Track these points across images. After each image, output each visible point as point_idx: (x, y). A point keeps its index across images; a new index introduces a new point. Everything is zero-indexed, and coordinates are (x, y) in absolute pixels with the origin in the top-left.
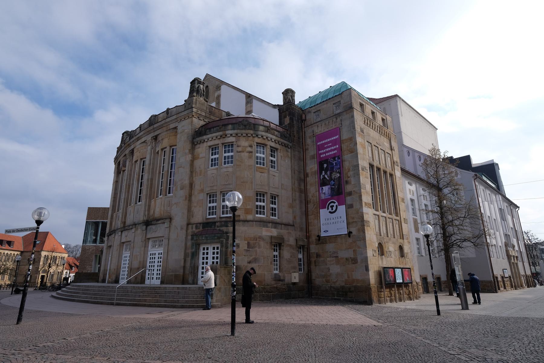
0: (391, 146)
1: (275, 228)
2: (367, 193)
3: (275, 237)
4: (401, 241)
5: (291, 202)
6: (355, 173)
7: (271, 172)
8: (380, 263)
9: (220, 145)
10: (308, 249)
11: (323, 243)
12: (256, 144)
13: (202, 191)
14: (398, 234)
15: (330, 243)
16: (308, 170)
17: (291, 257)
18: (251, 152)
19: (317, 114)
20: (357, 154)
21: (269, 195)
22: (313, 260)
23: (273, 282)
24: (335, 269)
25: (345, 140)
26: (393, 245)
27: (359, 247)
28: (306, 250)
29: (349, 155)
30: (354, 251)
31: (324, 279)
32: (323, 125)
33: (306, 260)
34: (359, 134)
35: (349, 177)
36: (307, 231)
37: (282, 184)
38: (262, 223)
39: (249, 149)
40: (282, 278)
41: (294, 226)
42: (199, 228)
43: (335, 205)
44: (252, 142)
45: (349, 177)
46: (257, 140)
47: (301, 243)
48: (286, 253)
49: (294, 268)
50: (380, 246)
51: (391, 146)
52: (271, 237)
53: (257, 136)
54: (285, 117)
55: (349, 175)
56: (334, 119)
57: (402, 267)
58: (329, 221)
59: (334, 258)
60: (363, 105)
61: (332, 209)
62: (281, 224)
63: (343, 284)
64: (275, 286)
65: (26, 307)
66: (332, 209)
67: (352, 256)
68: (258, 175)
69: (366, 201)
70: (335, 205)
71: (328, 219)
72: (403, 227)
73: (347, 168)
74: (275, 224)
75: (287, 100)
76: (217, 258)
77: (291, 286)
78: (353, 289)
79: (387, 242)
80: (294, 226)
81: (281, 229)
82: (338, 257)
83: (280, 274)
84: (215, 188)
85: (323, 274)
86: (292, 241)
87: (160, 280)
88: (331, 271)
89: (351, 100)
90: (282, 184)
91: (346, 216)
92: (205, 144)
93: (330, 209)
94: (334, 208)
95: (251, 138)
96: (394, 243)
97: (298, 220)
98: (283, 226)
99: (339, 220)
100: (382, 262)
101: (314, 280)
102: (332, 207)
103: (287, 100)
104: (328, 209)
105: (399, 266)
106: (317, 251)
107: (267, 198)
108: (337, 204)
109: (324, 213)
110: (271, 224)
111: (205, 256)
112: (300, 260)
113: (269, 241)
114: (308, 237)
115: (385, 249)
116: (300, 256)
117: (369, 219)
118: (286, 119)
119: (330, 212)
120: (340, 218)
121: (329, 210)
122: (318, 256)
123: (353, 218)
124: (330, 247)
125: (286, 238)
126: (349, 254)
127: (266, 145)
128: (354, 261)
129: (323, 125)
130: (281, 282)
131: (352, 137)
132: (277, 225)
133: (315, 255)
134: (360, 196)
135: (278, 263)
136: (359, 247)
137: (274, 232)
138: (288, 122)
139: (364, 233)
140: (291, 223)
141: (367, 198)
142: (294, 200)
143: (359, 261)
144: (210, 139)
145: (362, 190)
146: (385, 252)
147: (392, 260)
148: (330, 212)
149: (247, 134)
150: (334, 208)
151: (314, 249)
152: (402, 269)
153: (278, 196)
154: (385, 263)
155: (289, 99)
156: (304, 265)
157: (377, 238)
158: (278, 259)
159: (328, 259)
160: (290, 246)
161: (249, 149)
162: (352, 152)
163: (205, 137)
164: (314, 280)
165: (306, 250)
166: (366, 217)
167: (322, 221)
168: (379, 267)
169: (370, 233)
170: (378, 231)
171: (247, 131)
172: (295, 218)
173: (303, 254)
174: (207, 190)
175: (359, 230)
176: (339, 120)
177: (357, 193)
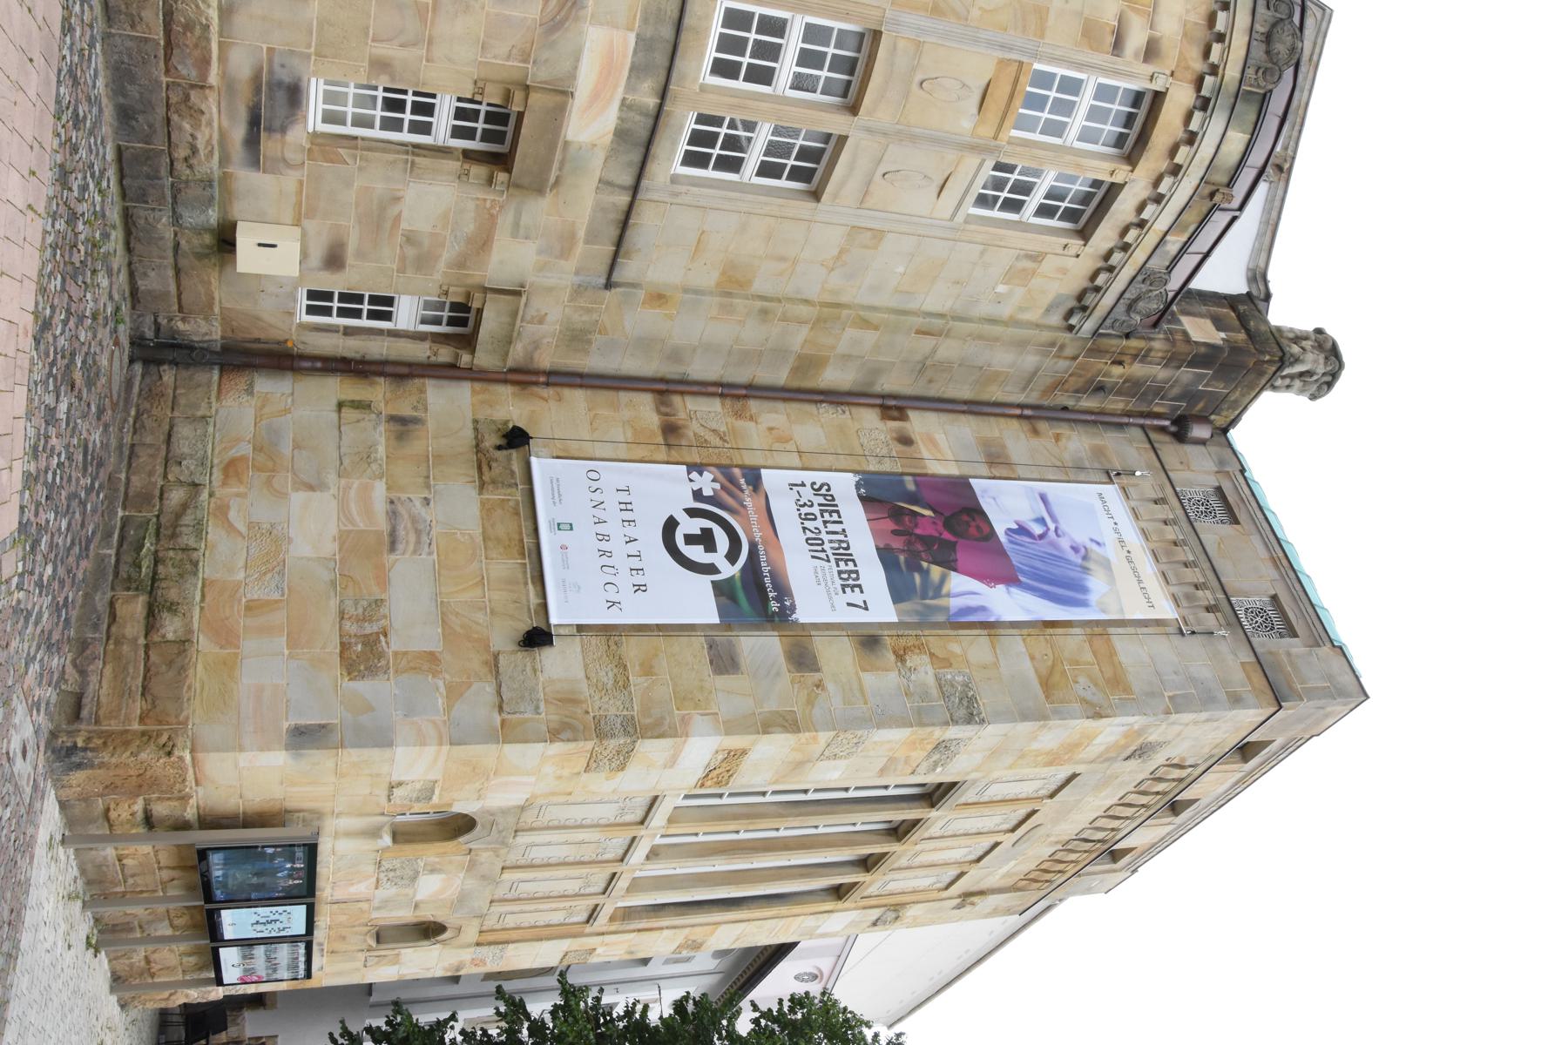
0: (981, 893)
1: (621, 134)
2: (799, 765)
3: (558, 114)
4: (471, 934)
5: (759, 286)
6: (925, 696)
7: (972, 161)
8: (345, 823)
10: (450, 372)
11: (482, 462)
12: (1157, 86)
14: (510, 921)
15: (487, 510)
16: (920, 423)
17: (410, 239)
18: (1118, 46)
19: (1215, 503)
20: (1042, 717)
21: (837, 123)
22: (377, 391)
23: (242, 64)
24: (312, 525)
25: (1112, 653)
26: (452, 892)
27: (454, 693)
28: (445, 354)
29: (1027, 667)
30: (432, 657)
31: (245, 449)
32: (1171, 533)
33: (377, 349)
34: (1139, 733)
35: (900, 658)
36: (561, 378)
37: (879, 235)
38: (667, 32)
39: (1136, 39)
40: (268, 145)
41: (609, 285)
43: (718, 558)
44: (1171, 64)
45: (900, 658)
46: (1180, 97)
47: (491, 322)
48: (438, 201)
49: (334, 260)
50: (458, 826)
51: (981, 893)
52: (562, 93)
53: (1204, 104)
54: (1219, 324)
55: (913, 660)
56: (1206, 597)
57: (319, 935)
58: (612, 513)
59: (383, 524)
60: (1245, 759)
61: (690, 540)
62: (635, 189)
63: (207, 570)
64: (213, 78)
66: (690, 540)
67: (394, 644)
68: (978, 66)
69: (752, 756)
70: (718, 558)
71: (626, 507)
72: (546, 945)
73: (955, 648)
74: (641, 141)
75: (1295, 349)
77: (213, 216)
78: (171, 627)
79: (472, 865)
80: (609, 285)
81: (604, 183)
82: (393, 546)
83: (296, 136)
85: (286, 449)
86: (511, 258)
88: (298, 498)
89: (1311, 693)
90: (879, 235)
91: (659, 627)
93: (694, 526)
94: (696, 553)
95: (1198, 66)
96: (462, 899)
97: (639, 319)
98: (624, 199)
99: (625, 581)
100: (349, 834)
101: (250, 391)
102: (706, 540)
103: (1295, 349)
104: (692, 513)
105: (322, 922)
106: (431, 425)
108: (728, 571)
109: (668, 489)
110: (652, 102)
112: (383, 306)
113: (538, 74)
114: (524, 377)
115: (431, 852)
116: (406, 314)
117: (633, 769)
118: (1208, 324)
119: (670, 525)
120: (639, 588)
121: (682, 518)
122: (403, 426)
123: (648, 670)
124: (459, 506)
125: (539, 211)
126: (411, 617)
127: (1132, 159)
128: (363, 654)
129: (1171, 533)
130: (239, 133)
131: (1127, 689)
132: (636, 157)
133: (406, 411)
134: (790, 724)
135: (377, 133)
136: (454, 693)
137: (591, 125)
138: (1196, 336)
139: (554, 735)
140: (629, 270)
141: (768, 762)
142: (767, 308)
143: (364, 687)
145: (824, 737)
146: (409, 849)
147: (362, 888)
148: (670, 525)
149: (1220, 38)
151: (450, 407)
152: (307, 939)
153: (816, 195)
154: (345, 846)
155: (1297, 360)
156: (348, 331)
157: (505, 812)
158: (405, 136)
159: (380, 490)
160: (482, 243)
161: (1136, 39)
162: (1047, 684)
164: (250, 391)
165: (445, 354)
166: (651, 750)
167: (614, 474)
168: (319, 815)
169: (549, 769)
170: (544, 820)
171: (1239, 42)
172: (659, 298)
173: (421, 337)
176: (1210, 620)
177: (810, 702)
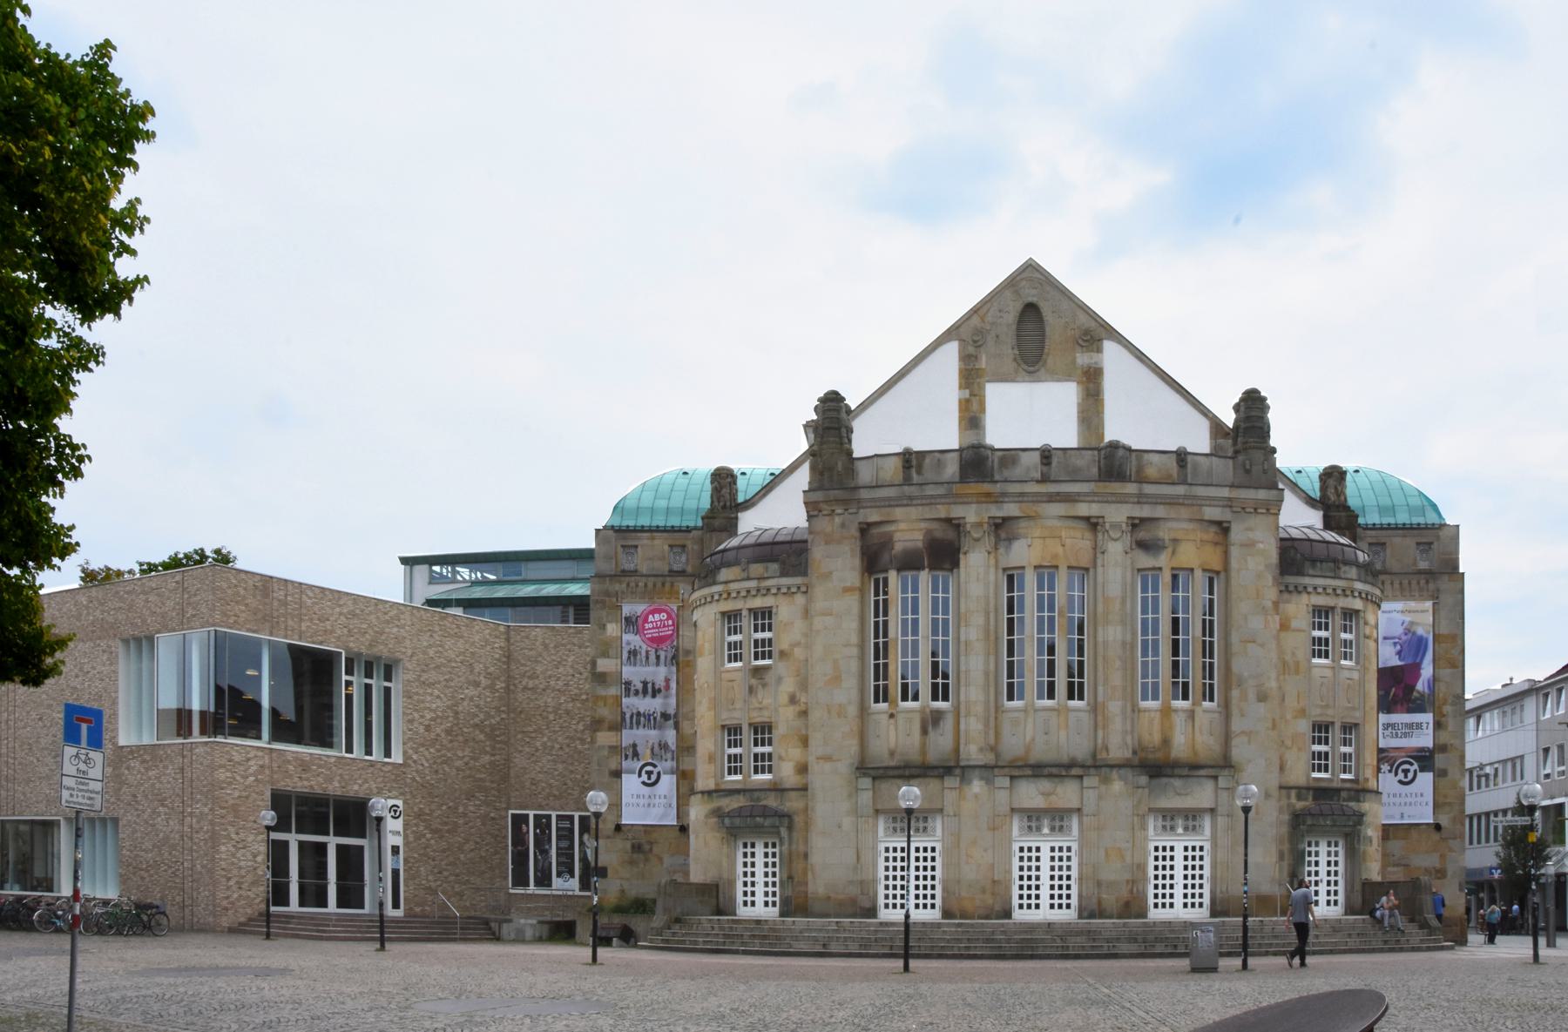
9: (745, 613)
13: (1302, 713)
27: (1451, 850)
42: (1306, 799)
43: (1412, 769)
65: (79, 986)
70: (1412, 769)
76: (774, 855)
84: (1330, 712)
87: (777, 909)
92: (1305, 597)
94: (1410, 776)
102: (1406, 772)
107: (747, 736)
108: (1416, 766)
111: (1333, 868)
119: (1400, 782)
136: (1451, 850)
143: (1449, 873)
144: (784, 590)
148: (1400, 782)
150: (1410, 776)
163: (1307, 580)
174: (1316, 714)
175: (1454, 820)
